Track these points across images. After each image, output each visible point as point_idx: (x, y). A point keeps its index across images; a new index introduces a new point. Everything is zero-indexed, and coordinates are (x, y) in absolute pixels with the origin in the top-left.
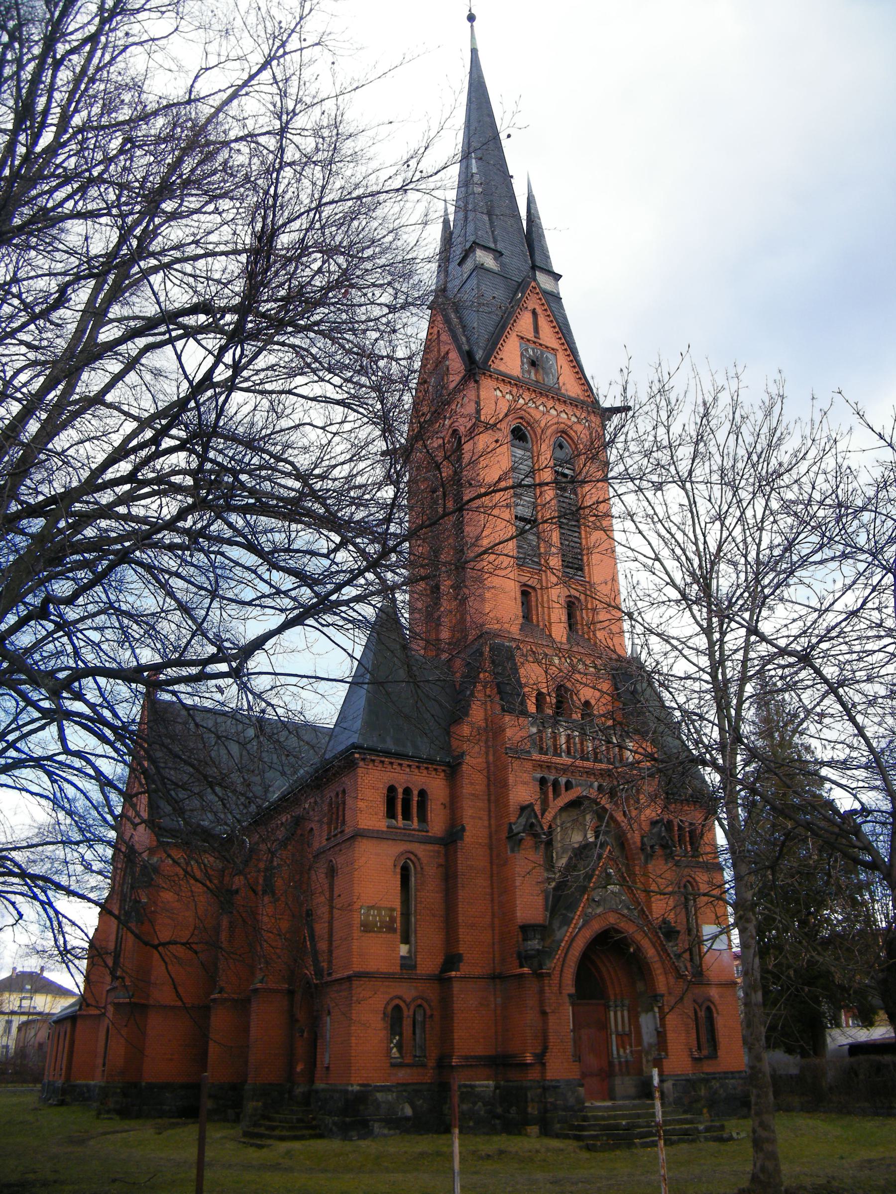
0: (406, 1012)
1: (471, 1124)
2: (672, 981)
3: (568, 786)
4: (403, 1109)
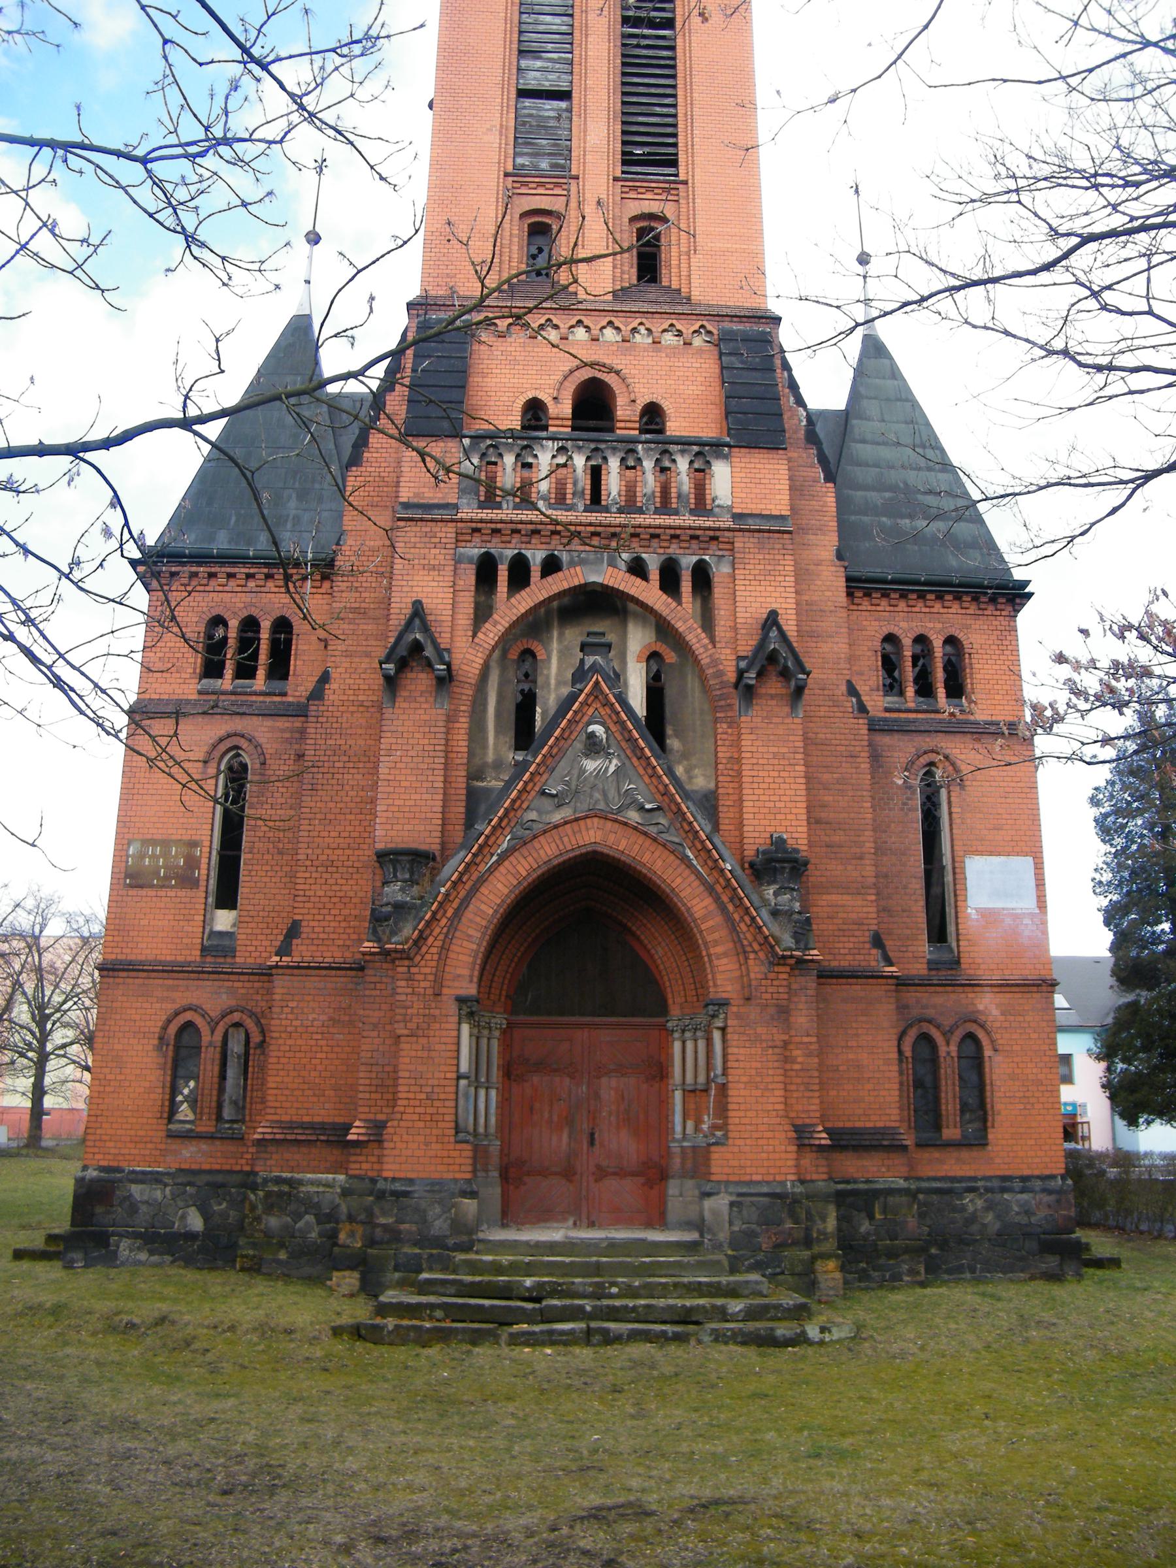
0: (206, 1037)
1: (283, 1256)
2: (756, 969)
3: (551, 566)
4: (183, 1217)
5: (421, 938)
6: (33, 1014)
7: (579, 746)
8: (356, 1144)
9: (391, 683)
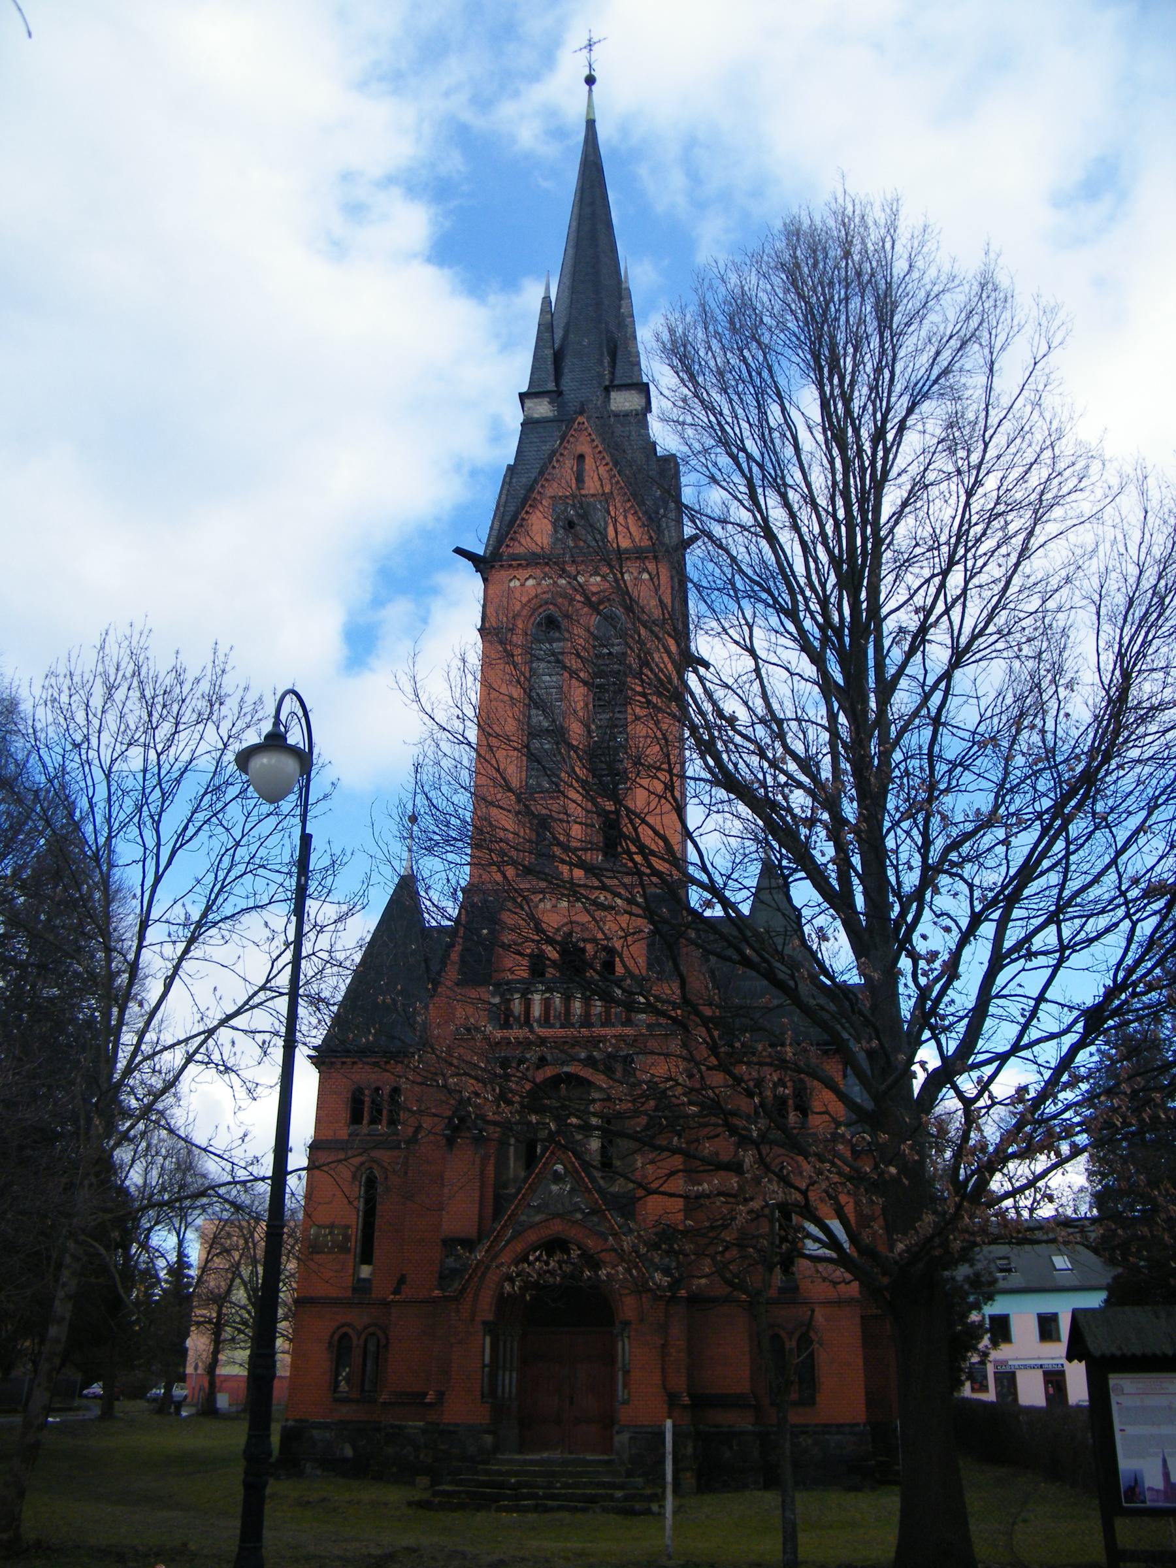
0: (355, 1341)
1: (394, 1470)
5: (462, 1292)
6: (249, 1295)
7: (549, 1177)
8: (430, 1404)
9: (450, 1142)
